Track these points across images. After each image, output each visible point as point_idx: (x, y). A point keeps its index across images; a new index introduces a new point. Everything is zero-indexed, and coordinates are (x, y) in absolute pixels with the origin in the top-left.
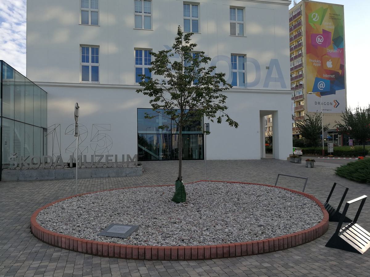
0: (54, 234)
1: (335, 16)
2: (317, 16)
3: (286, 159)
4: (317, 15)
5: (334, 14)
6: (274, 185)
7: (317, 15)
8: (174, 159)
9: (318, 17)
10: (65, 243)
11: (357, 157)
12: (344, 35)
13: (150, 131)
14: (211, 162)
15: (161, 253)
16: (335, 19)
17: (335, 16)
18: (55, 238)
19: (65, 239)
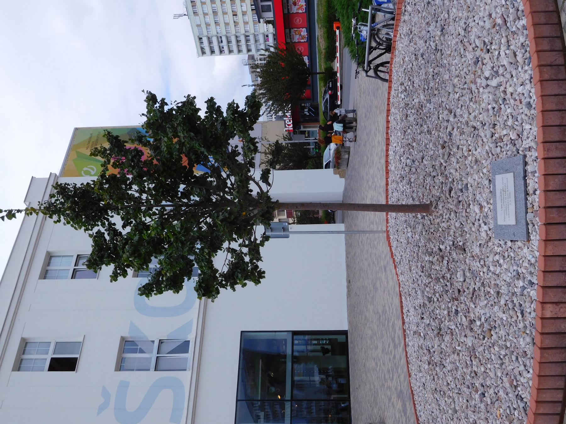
0: (533, 416)
1: (92, 141)
2: (89, 168)
3: (343, 180)
4: (85, 169)
5: (89, 142)
6: (386, 85)
7: (85, 169)
8: (346, 396)
9: (88, 166)
10: (557, 303)
11: (335, 31)
12: (127, 126)
13: (287, 389)
14: (350, 323)
15: (546, 30)
16: (97, 140)
17: (92, 141)
18: (541, 411)
19: (548, 305)
